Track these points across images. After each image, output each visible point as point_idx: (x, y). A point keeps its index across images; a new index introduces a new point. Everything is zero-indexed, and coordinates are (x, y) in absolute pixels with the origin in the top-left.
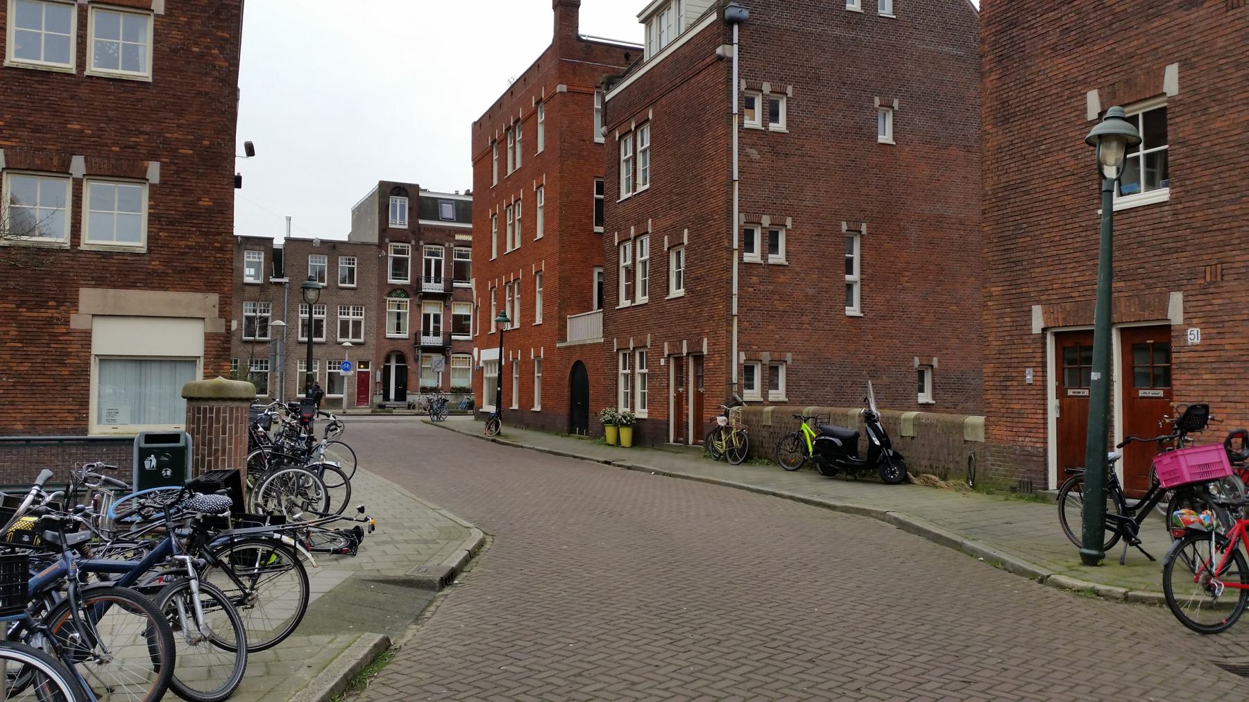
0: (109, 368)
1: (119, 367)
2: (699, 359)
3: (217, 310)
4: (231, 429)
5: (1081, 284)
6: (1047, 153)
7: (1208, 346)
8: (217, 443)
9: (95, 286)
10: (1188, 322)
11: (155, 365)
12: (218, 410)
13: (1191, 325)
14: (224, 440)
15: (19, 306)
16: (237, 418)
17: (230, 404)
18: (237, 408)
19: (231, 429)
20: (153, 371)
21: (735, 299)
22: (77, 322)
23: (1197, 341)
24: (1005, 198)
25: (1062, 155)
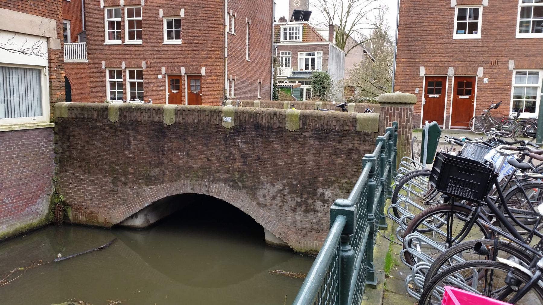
2: (194, 77)
3: (56, 32)
5: (443, 61)
6: (431, 14)
7: (490, 83)
10: (484, 76)
13: (485, 77)
21: (226, 49)
23: (487, 82)
24: (409, 27)
25: (438, 16)
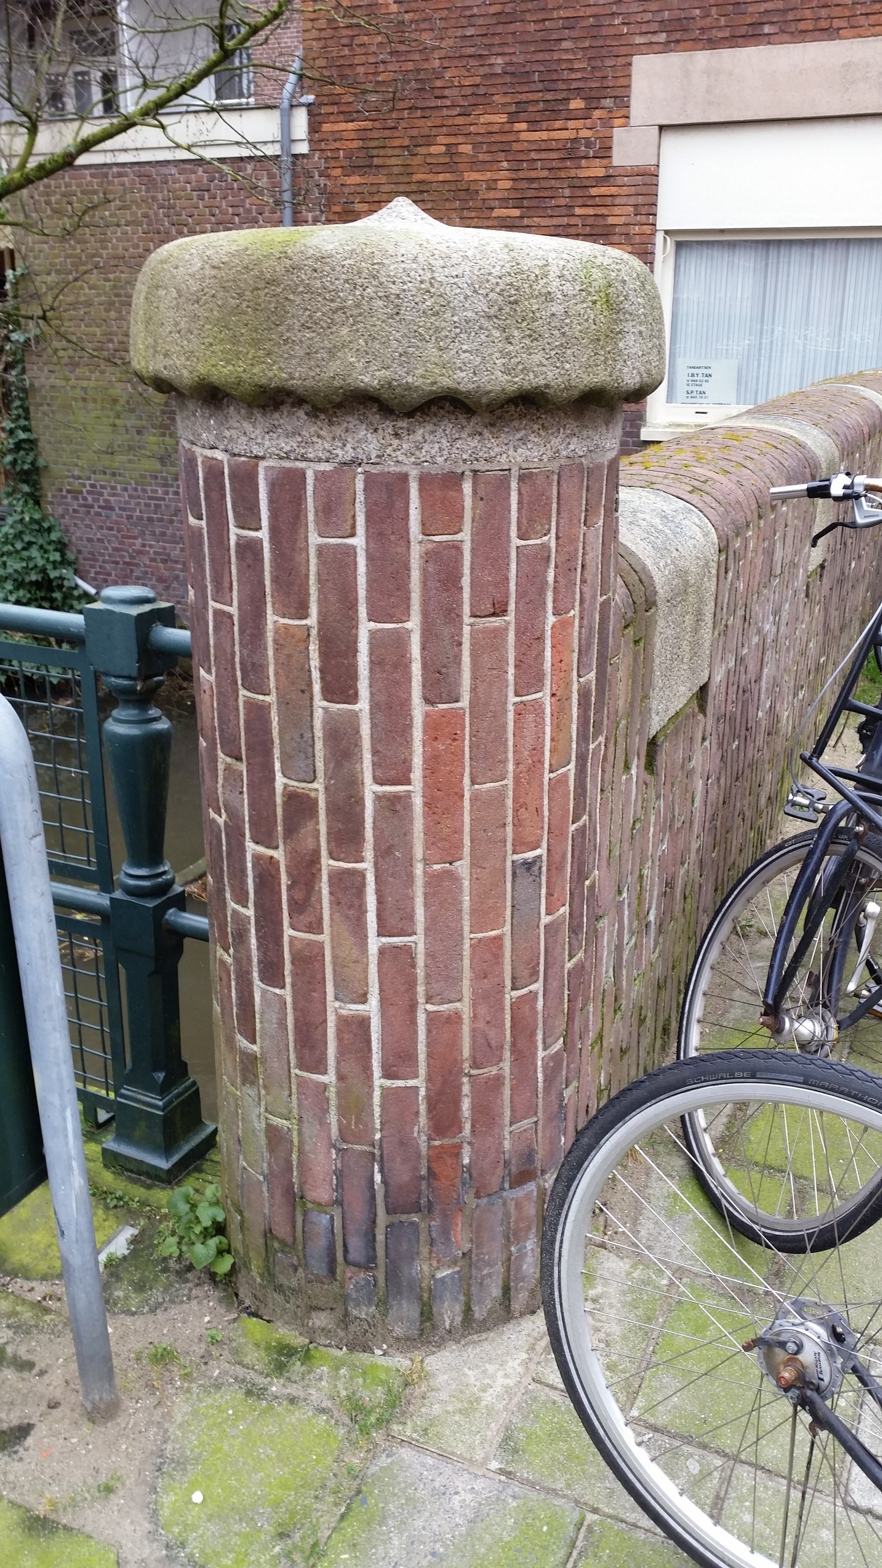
0: (694, 262)
1: (721, 259)
4: (390, 657)
8: (299, 756)
9: (667, 47)
11: (797, 256)
12: (288, 486)
14: (342, 741)
15: (513, 117)
16: (444, 569)
17: (366, 442)
18: (442, 487)
19: (390, 657)
20: (795, 268)
22: (628, 148)
